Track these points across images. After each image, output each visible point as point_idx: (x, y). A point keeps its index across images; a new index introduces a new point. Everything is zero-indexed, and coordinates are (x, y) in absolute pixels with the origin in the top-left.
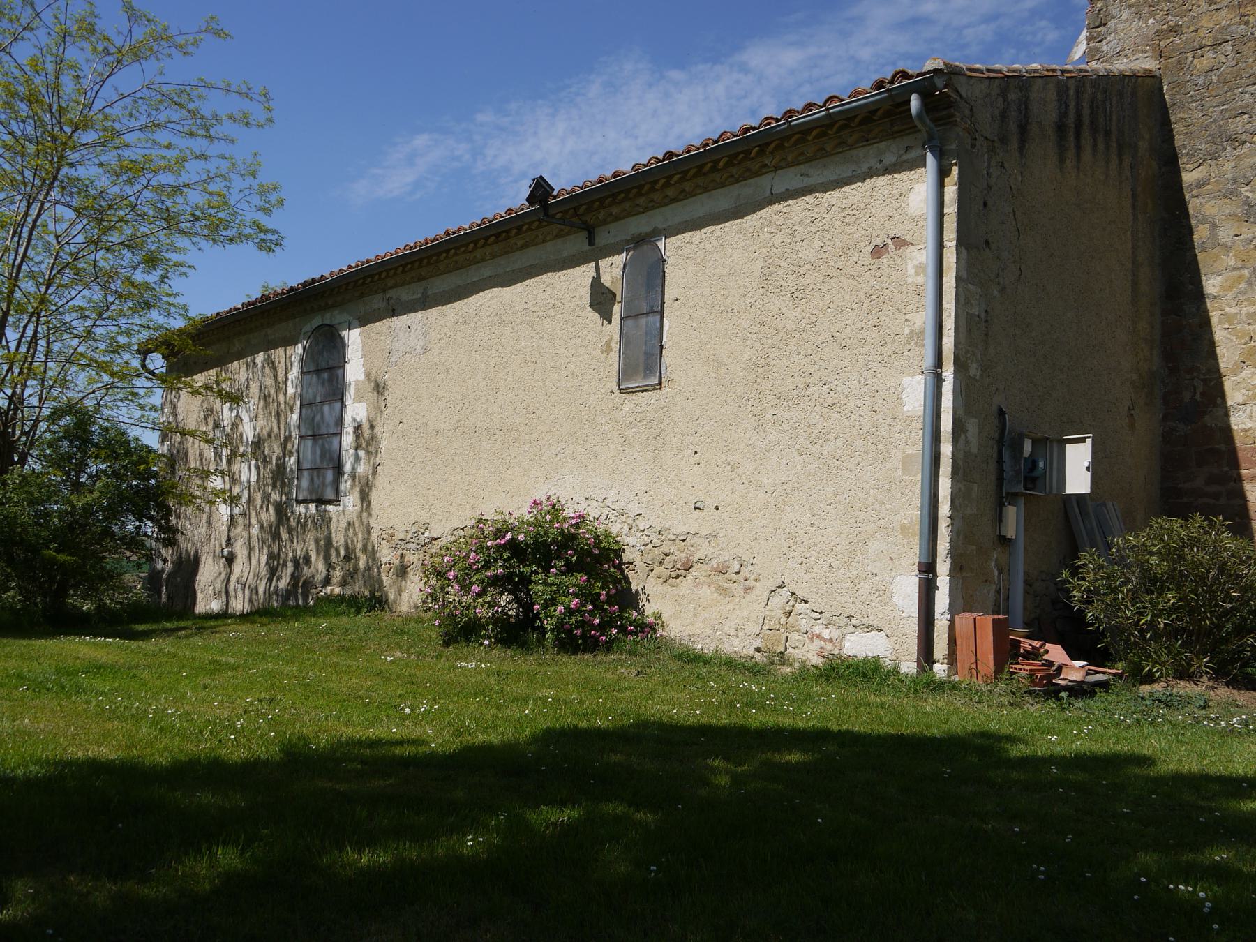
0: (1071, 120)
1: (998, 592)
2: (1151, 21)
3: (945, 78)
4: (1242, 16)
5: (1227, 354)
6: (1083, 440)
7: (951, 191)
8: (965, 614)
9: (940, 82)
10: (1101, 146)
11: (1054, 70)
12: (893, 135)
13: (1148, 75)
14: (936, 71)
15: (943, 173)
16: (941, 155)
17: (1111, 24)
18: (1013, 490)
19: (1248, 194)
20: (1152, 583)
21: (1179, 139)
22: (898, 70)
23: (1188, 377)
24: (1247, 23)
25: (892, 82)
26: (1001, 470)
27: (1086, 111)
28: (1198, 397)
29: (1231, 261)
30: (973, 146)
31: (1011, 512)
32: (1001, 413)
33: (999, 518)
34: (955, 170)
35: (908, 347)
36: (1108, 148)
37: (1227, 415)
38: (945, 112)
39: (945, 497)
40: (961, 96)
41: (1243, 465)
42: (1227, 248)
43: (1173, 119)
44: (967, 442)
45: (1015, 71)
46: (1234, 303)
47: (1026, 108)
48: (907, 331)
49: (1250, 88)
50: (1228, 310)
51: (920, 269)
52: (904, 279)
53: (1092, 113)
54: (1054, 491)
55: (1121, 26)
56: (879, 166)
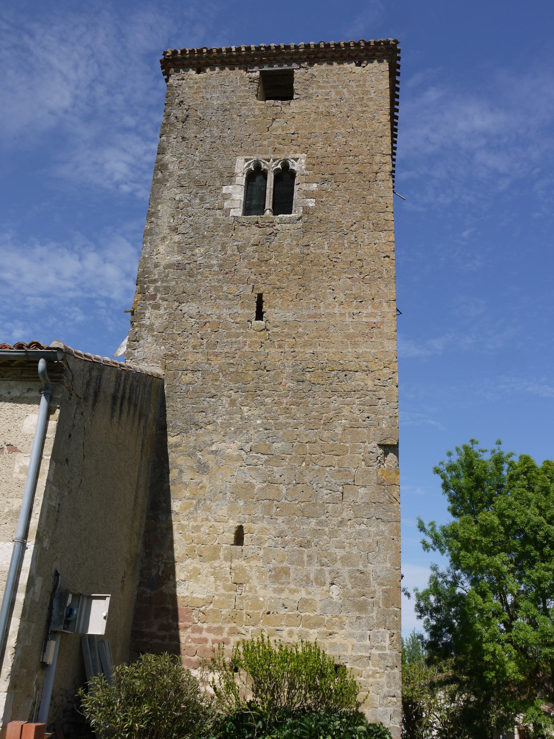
0: (120, 395)
1: (34, 704)
2: (163, 347)
3: (63, 355)
4: (208, 360)
5: (179, 549)
6: (104, 598)
7: (53, 424)
8: (14, 722)
9: (60, 356)
10: (132, 412)
11: (116, 364)
12: (21, 379)
13: (158, 377)
14: (58, 349)
15: (50, 411)
16: (51, 400)
17: (141, 342)
18: (56, 629)
19: (200, 457)
20: (134, 699)
21: (169, 417)
22: (35, 341)
23: (156, 560)
24: (210, 364)
25: (29, 347)
26: (50, 615)
27: (128, 391)
28: (160, 573)
29: (187, 494)
30: (70, 399)
31: (53, 646)
32: (57, 574)
33: (44, 649)
34: (58, 412)
35: (5, 521)
36: (134, 414)
37: (175, 587)
38: (58, 375)
39: (13, 632)
40: (69, 368)
41: (180, 619)
42: (186, 485)
43: (167, 404)
44: (34, 593)
45: (98, 359)
46: (186, 518)
47: (100, 382)
48: (7, 510)
49: (207, 399)
50: (182, 522)
51: (23, 470)
52: (11, 474)
53: (130, 392)
54: (80, 632)
55: (147, 345)
56: (7, 395)
